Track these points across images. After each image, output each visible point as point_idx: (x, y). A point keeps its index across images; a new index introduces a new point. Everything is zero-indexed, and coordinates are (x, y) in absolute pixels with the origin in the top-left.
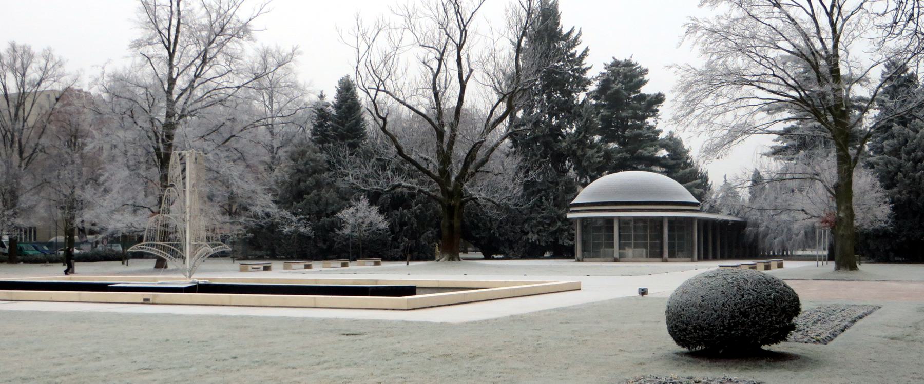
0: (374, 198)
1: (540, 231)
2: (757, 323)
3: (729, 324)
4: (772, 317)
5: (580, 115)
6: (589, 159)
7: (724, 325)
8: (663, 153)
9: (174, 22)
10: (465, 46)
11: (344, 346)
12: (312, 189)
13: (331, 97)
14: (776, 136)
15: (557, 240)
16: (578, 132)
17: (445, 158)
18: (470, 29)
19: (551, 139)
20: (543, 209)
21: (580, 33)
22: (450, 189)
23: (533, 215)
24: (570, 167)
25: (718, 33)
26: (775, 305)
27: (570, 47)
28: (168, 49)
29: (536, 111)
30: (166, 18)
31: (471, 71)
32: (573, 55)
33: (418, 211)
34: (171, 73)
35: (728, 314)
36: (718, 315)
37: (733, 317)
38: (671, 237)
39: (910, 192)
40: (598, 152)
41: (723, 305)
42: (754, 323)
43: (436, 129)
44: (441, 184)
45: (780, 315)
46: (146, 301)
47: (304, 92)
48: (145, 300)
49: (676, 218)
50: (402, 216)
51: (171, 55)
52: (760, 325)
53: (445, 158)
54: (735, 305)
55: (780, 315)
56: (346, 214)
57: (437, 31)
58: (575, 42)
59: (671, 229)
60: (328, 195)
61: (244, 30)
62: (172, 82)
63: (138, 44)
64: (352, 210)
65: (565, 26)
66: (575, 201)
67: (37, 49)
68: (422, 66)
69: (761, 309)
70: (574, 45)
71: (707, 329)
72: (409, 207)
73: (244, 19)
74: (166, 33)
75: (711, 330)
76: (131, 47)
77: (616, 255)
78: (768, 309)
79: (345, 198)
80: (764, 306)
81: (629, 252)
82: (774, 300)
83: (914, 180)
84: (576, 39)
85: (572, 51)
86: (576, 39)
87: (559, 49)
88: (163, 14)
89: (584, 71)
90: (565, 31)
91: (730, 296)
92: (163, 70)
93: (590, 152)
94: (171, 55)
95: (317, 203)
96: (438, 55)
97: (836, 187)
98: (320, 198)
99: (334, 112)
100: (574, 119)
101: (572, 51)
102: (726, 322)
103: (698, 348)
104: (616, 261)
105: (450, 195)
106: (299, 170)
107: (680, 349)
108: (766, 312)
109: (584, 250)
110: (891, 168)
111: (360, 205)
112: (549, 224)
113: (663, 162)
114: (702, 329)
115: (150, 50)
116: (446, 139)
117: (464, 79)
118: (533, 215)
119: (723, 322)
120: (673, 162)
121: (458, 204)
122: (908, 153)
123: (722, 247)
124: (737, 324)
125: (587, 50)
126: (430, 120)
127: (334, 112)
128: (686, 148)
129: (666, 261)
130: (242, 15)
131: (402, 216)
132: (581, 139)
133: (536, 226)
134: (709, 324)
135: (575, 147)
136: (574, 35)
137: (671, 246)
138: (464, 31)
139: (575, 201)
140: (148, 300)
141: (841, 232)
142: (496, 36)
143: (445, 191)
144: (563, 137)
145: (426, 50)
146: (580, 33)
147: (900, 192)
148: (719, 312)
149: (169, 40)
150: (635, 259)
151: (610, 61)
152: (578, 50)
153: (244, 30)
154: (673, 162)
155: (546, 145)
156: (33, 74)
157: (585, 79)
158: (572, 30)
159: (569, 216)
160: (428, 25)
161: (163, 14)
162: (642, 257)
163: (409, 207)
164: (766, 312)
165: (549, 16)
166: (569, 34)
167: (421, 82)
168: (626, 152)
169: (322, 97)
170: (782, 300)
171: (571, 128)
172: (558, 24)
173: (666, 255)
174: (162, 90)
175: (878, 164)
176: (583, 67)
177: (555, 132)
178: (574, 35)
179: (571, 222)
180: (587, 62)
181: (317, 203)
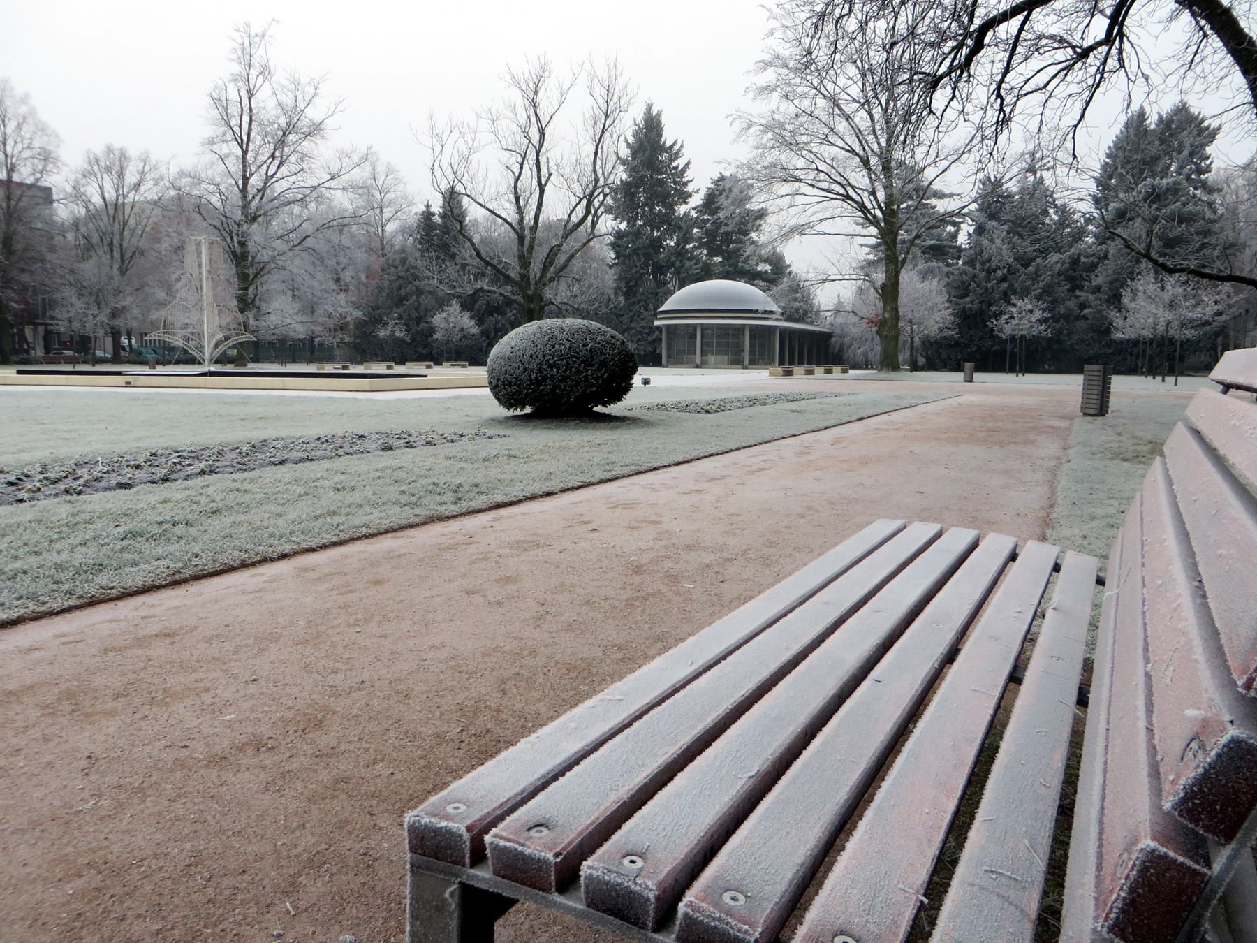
0: (468, 304)
1: (639, 340)
2: (568, 377)
3: (536, 378)
4: (587, 371)
5: (680, 228)
6: (687, 270)
7: (531, 380)
8: (764, 267)
9: (246, 119)
10: (543, 149)
11: (986, 503)
12: (411, 295)
13: (437, 207)
14: (868, 250)
15: (655, 349)
16: (678, 244)
17: (525, 262)
18: (547, 132)
19: (651, 251)
20: (642, 319)
21: (682, 146)
22: (530, 293)
23: (632, 325)
24: (671, 279)
25: (772, 126)
26: (592, 357)
27: (672, 160)
28: (241, 146)
29: (640, 223)
30: (236, 114)
31: (550, 174)
32: (676, 168)
33: (512, 318)
34: (245, 171)
35: (534, 366)
36: (526, 369)
37: (540, 370)
38: (751, 345)
39: (982, 302)
40: (696, 264)
41: (531, 356)
42: (564, 378)
43: (517, 233)
44: (521, 289)
45: (598, 369)
46: (128, 384)
47: (412, 204)
48: (127, 383)
49: (758, 326)
50: (497, 322)
51: (245, 153)
52: (572, 380)
53: (525, 262)
54: (544, 356)
55: (598, 369)
56: (438, 320)
57: (519, 134)
58: (677, 155)
59: (751, 337)
60: (425, 301)
61: (315, 130)
62: (246, 179)
63: (211, 142)
64: (444, 315)
65: (668, 137)
66: (662, 309)
67: (133, 152)
68: (504, 170)
69: (575, 362)
70: (676, 158)
71: (515, 384)
72: (503, 314)
73: (317, 119)
74: (237, 129)
75: (519, 386)
76: (203, 144)
77: (698, 361)
78: (582, 362)
79: (442, 303)
80: (579, 358)
81: (712, 359)
82: (591, 351)
83: (986, 289)
84: (679, 151)
85: (674, 164)
86: (679, 151)
87: (662, 161)
88: (234, 110)
89: (686, 184)
90: (668, 144)
91: (540, 346)
92: (236, 168)
93: (688, 264)
94: (245, 153)
95: (417, 309)
96: (520, 159)
97: (883, 287)
98: (419, 304)
99: (440, 221)
100: (675, 232)
101: (674, 164)
102: (533, 376)
103: (528, 410)
104: (698, 367)
105: (530, 299)
106: (399, 277)
107: (503, 412)
108: (580, 365)
109: (669, 356)
110: (965, 278)
111: (451, 310)
112: (648, 334)
113: (764, 276)
114: (510, 385)
115: (224, 149)
116: (527, 242)
117: (543, 183)
118: (632, 325)
119: (530, 376)
120: (774, 276)
121: (537, 308)
122: (983, 263)
123: (810, 353)
124: (544, 379)
125: (689, 163)
126: (510, 224)
127: (440, 221)
128: (788, 263)
129: (747, 368)
130: (313, 114)
131: (497, 322)
132: (680, 252)
133: (636, 335)
134: (516, 379)
135: (673, 259)
136: (676, 148)
137: (752, 352)
138: (542, 135)
139: (662, 309)
140: (129, 383)
141: (885, 333)
142: (581, 142)
143: (526, 296)
144: (664, 248)
145: (507, 154)
146: (682, 146)
147: (972, 302)
148: (526, 365)
149: (241, 138)
150: (716, 366)
151: (716, 176)
152: (680, 163)
153: (315, 130)
154: (774, 276)
155: (648, 257)
156: (131, 177)
157: (686, 192)
158: (675, 143)
159: (656, 323)
160: (509, 130)
161: (234, 110)
162: (723, 363)
163: (503, 314)
164: (580, 365)
165: (652, 129)
166: (672, 146)
167: (503, 189)
168: (730, 266)
169: (428, 206)
170: (601, 353)
171: (671, 239)
172: (661, 136)
173: (746, 362)
174: (236, 189)
175: (953, 274)
176: (685, 180)
177: (656, 244)
178: (676, 148)
179: (659, 328)
180: (688, 175)
181: (417, 309)
